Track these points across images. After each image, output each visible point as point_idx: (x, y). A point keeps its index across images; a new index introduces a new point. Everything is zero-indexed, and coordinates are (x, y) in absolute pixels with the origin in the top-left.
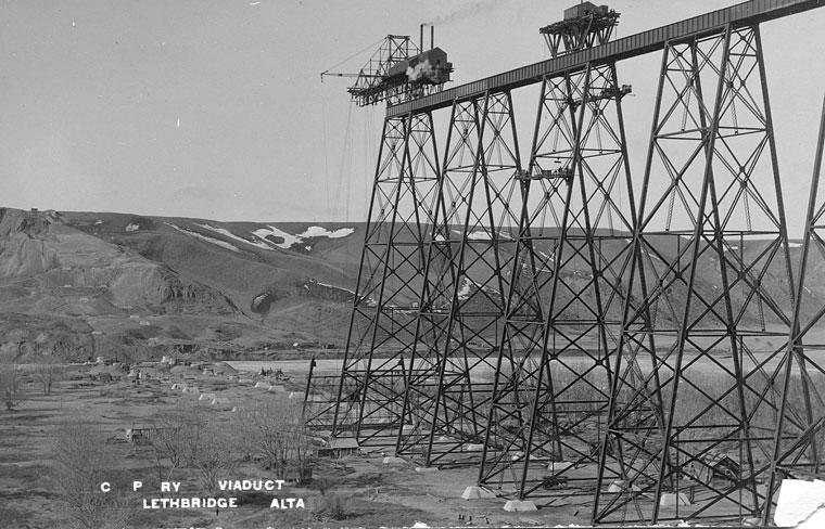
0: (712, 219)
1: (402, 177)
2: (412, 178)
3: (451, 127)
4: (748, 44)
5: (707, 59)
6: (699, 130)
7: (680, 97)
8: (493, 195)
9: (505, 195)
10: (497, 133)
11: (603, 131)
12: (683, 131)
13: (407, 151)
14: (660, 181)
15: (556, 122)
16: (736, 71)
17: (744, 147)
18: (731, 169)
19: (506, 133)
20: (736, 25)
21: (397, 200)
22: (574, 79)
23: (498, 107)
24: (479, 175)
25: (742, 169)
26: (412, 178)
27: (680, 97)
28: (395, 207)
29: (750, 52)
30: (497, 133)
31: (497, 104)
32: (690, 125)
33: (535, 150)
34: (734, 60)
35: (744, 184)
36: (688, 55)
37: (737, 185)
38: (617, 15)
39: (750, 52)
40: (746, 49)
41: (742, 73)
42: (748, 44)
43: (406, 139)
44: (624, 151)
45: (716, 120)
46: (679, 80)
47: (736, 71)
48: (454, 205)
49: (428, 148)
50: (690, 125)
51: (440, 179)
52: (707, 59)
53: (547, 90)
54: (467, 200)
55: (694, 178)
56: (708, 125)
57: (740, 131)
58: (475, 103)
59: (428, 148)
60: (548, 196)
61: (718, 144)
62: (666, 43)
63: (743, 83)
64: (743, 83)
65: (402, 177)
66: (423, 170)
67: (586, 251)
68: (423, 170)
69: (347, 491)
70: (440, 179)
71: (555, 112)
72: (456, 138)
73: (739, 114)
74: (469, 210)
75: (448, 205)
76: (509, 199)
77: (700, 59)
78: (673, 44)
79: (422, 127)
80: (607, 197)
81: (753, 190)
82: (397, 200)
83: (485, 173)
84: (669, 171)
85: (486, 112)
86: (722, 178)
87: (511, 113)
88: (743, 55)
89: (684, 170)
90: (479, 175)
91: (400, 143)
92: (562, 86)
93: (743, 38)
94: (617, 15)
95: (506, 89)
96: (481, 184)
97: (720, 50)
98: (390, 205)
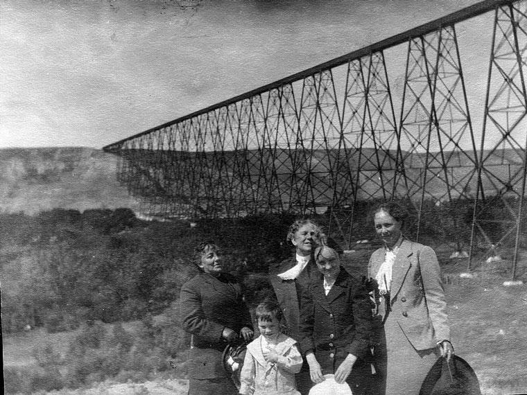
2: (254, 122)
3: (495, 27)
8: (287, 126)
9: (292, 125)
10: (325, 89)
11: (328, 96)
17: (450, 81)
19: (291, 100)
32: (423, 74)
34: (375, 65)
36: (420, 43)
37: (446, 101)
38: (12, 104)
43: (251, 105)
46: (354, 74)
49: (260, 109)
50: (423, 74)
51: (266, 120)
52: (429, 45)
57: (447, 75)
59: (260, 109)
65: (250, 122)
66: (259, 118)
68: (259, 118)
69: (19, 365)
70: (266, 120)
71: (309, 90)
72: (271, 103)
73: (447, 68)
75: (269, 130)
85: (282, 92)
91: (249, 107)
94: (12, 104)
95: (290, 83)
97: (436, 40)
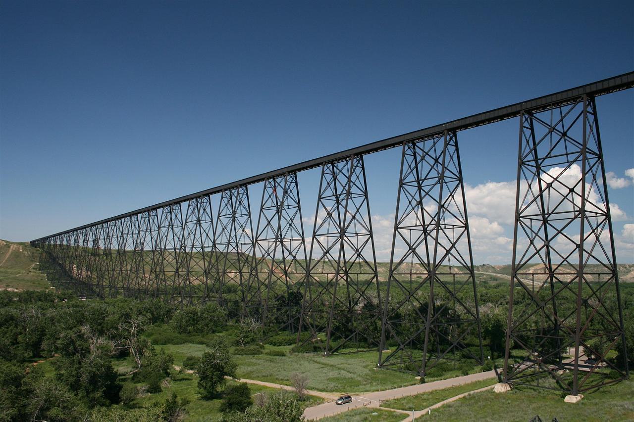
0: (234, 238)
1: (147, 230)
2: (150, 230)
4: (293, 179)
5: (279, 184)
6: (275, 206)
7: (270, 196)
10: (204, 210)
12: (226, 215)
13: (171, 219)
14: (264, 223)
15: (226, 205)
16: (289, 187)
18: (286, 220)
20: (241, 185)
21: (168, 233)
22: (233, 191)
23: (205, 201)
24: (170, 229)
25: (291, 219)
26: (150, 230)
27: (270, 196)
28: (144, 239)
29: (293, 181)
30: (204, 210)
31: (176, 207)
33: (186, 221)
35: (290, 225)
36: (273, 183)
39: (293, 181)
40: (292, 181)
41: (291, 188)
42: (293, 179)
43: (171, 213)
44: (299, 207)
45: (282, 202)
47: (289, 187)
48: (162, 237)
52: (279, 184)
53: (190, 203)
54: (194, 233)
55: (275, 223)
56: (279, 204)
57: (290, 207)
58: (170, 207)
59: (179, 216)
60: (223, 229)
61: (283, 212)
62: (404, 142)
63: (291, 191)
64: (291, 191)
65: (147, 230)
67: (236, 248)
71: (226, 202)
72: (164, 217)
74: (194, 237)
76: (208, 233)
77: (277, 184)
78: (268, 179)
79: (177, 208)
80: (207, 235)
81: (295, 227)
82: (168, 233)
83: (172, 228)
84: (222, 226)
85: (173, 209)
86: (284, 223)
87: (210, 203)
88: (243, 194)
89: (272, 219)
90: (170, 229)
92: (229, 194)
93: (291, 177)
96: (198, 227)
98: (164, 236)
